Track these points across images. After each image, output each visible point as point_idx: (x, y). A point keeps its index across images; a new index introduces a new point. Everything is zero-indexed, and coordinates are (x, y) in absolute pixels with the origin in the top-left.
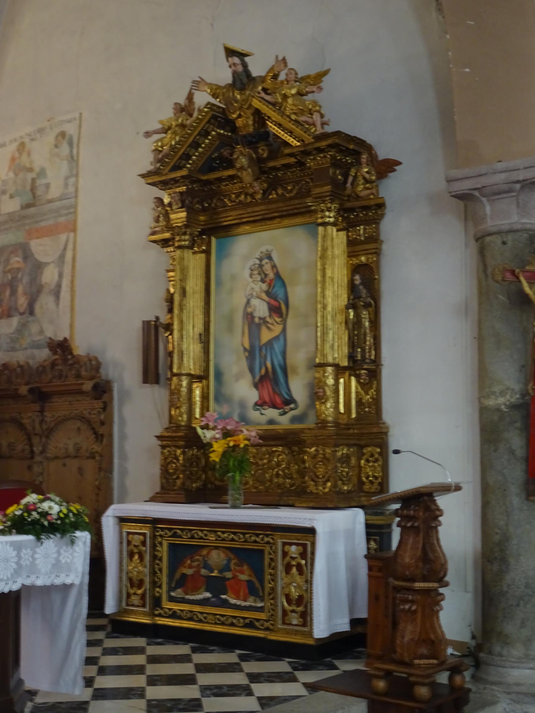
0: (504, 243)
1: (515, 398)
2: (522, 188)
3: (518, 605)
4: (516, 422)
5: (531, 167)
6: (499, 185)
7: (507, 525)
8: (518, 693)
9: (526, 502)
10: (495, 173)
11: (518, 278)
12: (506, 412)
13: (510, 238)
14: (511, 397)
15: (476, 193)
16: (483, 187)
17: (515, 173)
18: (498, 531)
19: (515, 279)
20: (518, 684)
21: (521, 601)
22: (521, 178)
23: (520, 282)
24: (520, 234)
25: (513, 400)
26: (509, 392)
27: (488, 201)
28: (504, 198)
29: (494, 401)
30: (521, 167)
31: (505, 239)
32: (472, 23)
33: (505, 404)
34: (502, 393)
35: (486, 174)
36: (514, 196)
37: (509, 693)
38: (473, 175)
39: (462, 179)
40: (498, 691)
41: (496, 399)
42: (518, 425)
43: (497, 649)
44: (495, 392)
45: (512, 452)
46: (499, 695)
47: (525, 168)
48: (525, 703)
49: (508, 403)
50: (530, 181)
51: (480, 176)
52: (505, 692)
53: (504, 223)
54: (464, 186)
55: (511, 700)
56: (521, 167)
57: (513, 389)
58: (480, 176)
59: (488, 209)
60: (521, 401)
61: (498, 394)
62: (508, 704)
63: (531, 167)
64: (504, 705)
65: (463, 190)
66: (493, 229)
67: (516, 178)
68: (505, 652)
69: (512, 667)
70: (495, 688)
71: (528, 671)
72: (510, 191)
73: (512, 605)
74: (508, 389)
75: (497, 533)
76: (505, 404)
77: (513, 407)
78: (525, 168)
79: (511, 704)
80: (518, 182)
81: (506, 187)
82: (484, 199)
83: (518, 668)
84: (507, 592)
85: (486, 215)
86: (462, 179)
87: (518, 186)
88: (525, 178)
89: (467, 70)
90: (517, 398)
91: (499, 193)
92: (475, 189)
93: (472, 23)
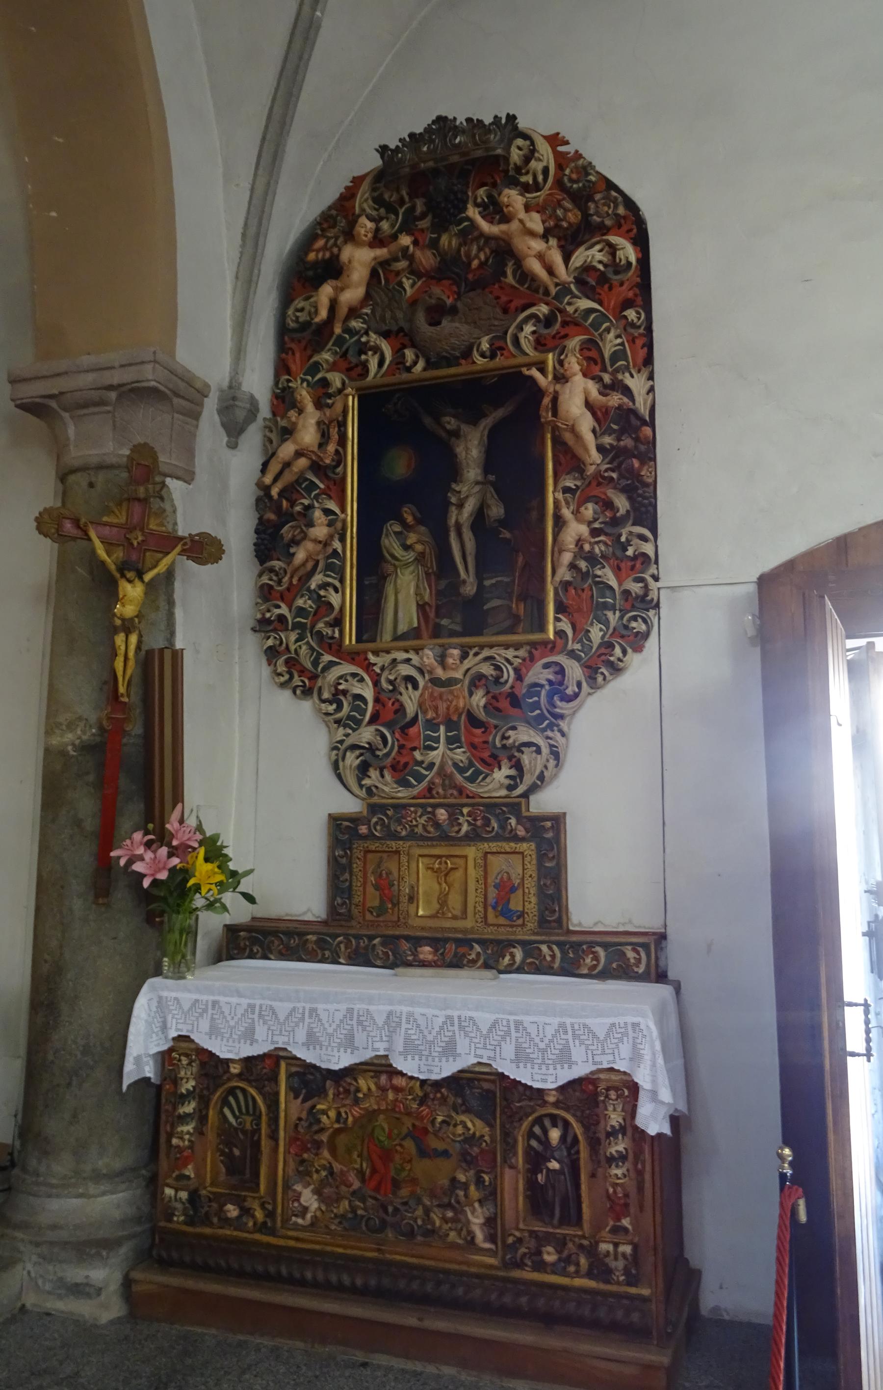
0: (91, 485)
1: (88, 734)
2: (120, 397)
3: (69, 1085)
4: (88, 773)
5: (130, 365)
6: (85, 392)
7: (61, 947)
8: (52, 1244)
9: (94, 906)
10: (80, 372)
11: (86, 533)
12: (73, 756)
13: (100, 478)
14: (84, 732)
15: (53, 404)
16: (61, 393)
17: (107, 373)
18: (47, 957)
19: (79, 533)
20: (54, 1227)
21: (74, 1078)
22: (115, 381)
23: (89, 539)
24: (117, 472)
25: (85, 737)
26: (82, 724)
27: (72, 417)
28: (94, 414)
29: (59, 739)
30: (117, 364)
31: (93, 479)
32: (61, 140)
33: (73, 744)
34: (71, 726)
35: (66, 373)
36: (109, 412)
37: (37, 1245)
38: (45, 373)
39: (30, 379)
40: (23, 1240)
41: (62, 736)
42: (91, 778)
43: (33, 1162)
44: (61, 724)
45: (78, 823)
46: (22, 1248)
47: (122, 366)
48: (61, 1262)
49: (77, 742)
50: (129, 387)
51: (58, 375)
52: (31, 1242)
53: (91, 453)
54: (33, 391)
55: (39, 1255)
56: (117, 364)
57: (86, 720)
58: (58, 375)
59: (71, 431)
60: (98, 739)
61: (64, 727)
62: (35, 1264)
63: (130, 365)
64: (29, 1267)
65: (32, 397)
66: (76, 463)
67: (108, 382)
68: (43, 1169)
69: (50, 1196)
70: (19, 1235)
71: (74, 1201)
72: (102, 403)
73: (58, 1085)
74: (80, 718)
75: (46, 961)
76: (73, 744)
77: (86, 748)
78: (122, 366)
79: (40, 1264)
80: (110, 388)
81: (95, 395)
82: (66, 415)
83: (58, 1196)
84: (52, 1062)
85: (68, 439)
86: (30, 379)
87: (113, 395)
88: (121, 382)
89: (54, 214)
90: (94, 735)
91: (85, 406)
92: (51, 397)
93: (61, 140)
